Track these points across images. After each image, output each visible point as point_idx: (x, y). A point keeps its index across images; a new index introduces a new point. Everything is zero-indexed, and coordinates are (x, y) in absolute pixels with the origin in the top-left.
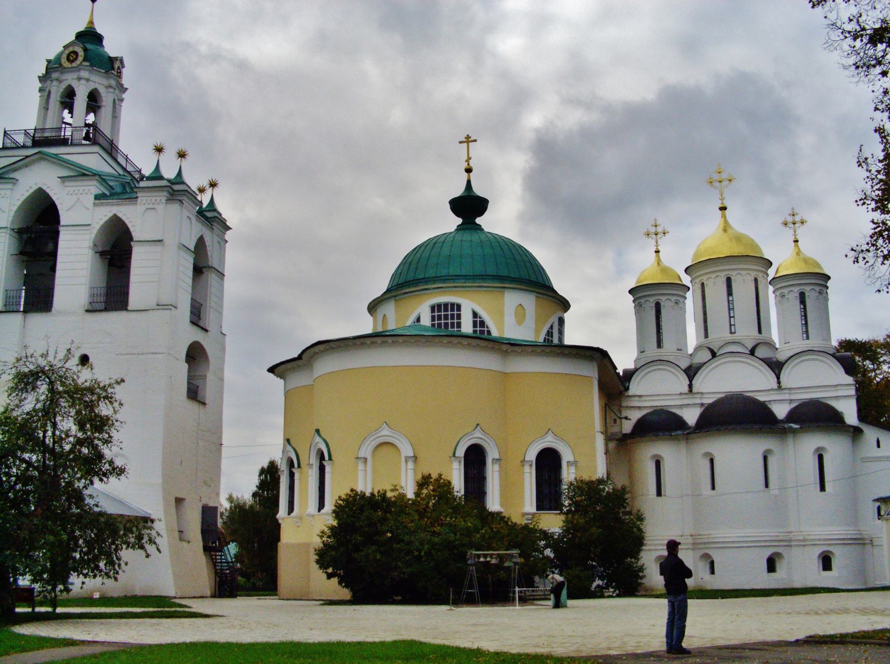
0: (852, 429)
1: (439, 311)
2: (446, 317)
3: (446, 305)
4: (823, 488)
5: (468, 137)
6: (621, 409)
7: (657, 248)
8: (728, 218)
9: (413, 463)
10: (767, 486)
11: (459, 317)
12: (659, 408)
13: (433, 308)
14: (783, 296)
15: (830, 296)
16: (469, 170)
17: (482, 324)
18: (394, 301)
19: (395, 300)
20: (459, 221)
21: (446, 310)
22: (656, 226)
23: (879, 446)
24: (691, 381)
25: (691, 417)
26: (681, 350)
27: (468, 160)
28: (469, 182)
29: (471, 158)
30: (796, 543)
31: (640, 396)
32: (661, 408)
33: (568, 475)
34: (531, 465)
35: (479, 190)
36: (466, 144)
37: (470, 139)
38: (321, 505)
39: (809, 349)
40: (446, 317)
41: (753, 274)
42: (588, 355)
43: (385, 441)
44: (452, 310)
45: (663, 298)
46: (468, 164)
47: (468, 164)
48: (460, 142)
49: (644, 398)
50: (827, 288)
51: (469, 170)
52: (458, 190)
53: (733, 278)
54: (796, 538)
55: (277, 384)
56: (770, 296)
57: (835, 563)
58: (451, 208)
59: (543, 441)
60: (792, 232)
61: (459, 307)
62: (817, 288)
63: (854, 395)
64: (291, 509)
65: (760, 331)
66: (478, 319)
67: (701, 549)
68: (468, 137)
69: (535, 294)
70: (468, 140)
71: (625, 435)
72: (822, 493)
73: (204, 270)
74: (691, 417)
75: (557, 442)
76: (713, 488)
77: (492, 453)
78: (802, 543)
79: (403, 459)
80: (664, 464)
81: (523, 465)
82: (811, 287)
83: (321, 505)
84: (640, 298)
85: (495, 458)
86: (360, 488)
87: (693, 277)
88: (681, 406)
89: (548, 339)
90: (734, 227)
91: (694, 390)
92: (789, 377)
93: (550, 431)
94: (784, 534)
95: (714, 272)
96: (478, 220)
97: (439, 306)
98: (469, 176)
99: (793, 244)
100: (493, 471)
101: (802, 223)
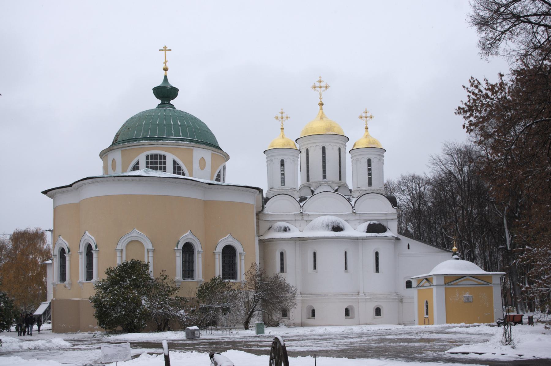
1: (152, 158)
2: (156, 163)
3: (156, 155)
4: (377, 270)
5: (165, 47)
6: (259, 221)
7: (282, 127)
8: (324, 111)
9: (152, 253)
13: (147, 157)
14: (357, 160)
15: (385, 162)
16: (166, 69)
17: (179, 168)
19: (121, 150)
20: (159, 102)
21: (156, 158)
22: (282, 113)
23: (409, 248)
27: (165, 62)
28: (166, 77)
29: (167, 62)
34: (219, 255)
35: (173, 82)
36: (164, 52)
37: (167, 49)
38: (89, 276)
39: (373, 192)
40: (156, 163)
41: (338, 146)
43: (132, 240)
44: (160, 159)
46: (166, 65)
47: (166, 65)
48: (170, 50)
50: (383, 157)
51: (166, 69)
52: (159, 82)
53: (326, 148)
55: (48, 201)
56: (348, 159)
58: (154, 93)
60: (364, 122)
61: (165, 157)
62: (378, 157)
63: (396, 219)
64: (63, 277)
65: (340, 179)
68: (165, 47)
70: (165, 49)
72: (377, 273)
77: (198, 247)
79: (146, 251)
82: (375, 156)
83: (89, 276)
84: (271, 156)
87: (353, 155)
89: (218, 179)
95: (315, 143)
97: (152, 156)
98: (166, 73)
99: (365, 130)
101: (371, 117)
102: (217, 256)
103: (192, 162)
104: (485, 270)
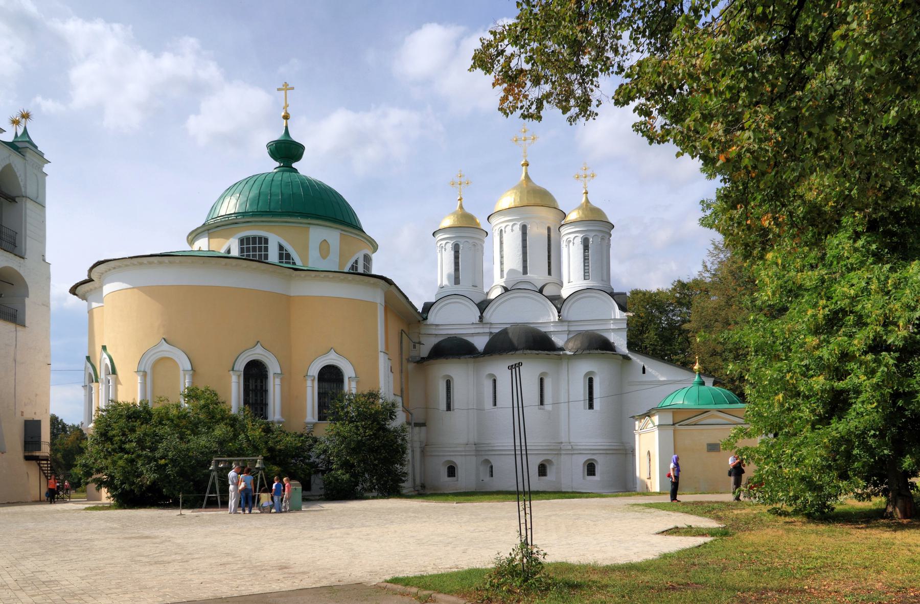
0: (621, 358)
1: (248, 243)
2: (254, 249)
3: (254, 238)
10: (542, 403)
11: (266, 249)
12: (452, 336)
13: (242, 241)
16: (286, 117)
17: (288, 256)
18: (207, 235)
19: (209, 233)
20: (277, 164)
23: (644, 372)
24: (482, 313)
25: (480, 343)
26: (476, 286)
30: (564, 452)
31: (437, 325)
32: (455, 335)
33: (350, 387)
35: (295, 136)
42: (372, 282)
44: (260, 243)
45: (462, 240)
48: (279, 90)
49: (441, 327)
52: (278, 135)
54: (565, 448)
57: (598, 470)
59: (325, 358)
61: (266, 241)
62: (600, 235)
66: (284, 252)
67: (482, 455)
68: (286, 84)
69: (340, 231)
71: (423, 359)
73: (17, 199)
74: (480, 343)
75: (339, 359)
76: (495, 404)
77: (273, 367)
78: (570, 452)
80: (453, 383)
81: (306, 380)
85: (186, 369)
86: (122, 398)
88: (473, 335)
90: (533, 181)
91: (484, 321)
92: (570, 312)
93: (259, 344)
94: (554, 444)
96: (294, 165)
97: (248, 239)
100: (274, 385)
102: (309, 383)
103: (308, 247)
104: (696, 363)
